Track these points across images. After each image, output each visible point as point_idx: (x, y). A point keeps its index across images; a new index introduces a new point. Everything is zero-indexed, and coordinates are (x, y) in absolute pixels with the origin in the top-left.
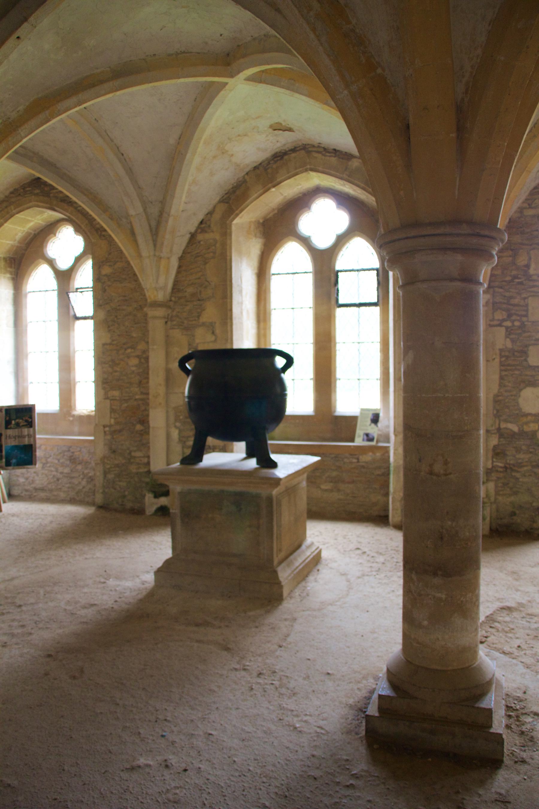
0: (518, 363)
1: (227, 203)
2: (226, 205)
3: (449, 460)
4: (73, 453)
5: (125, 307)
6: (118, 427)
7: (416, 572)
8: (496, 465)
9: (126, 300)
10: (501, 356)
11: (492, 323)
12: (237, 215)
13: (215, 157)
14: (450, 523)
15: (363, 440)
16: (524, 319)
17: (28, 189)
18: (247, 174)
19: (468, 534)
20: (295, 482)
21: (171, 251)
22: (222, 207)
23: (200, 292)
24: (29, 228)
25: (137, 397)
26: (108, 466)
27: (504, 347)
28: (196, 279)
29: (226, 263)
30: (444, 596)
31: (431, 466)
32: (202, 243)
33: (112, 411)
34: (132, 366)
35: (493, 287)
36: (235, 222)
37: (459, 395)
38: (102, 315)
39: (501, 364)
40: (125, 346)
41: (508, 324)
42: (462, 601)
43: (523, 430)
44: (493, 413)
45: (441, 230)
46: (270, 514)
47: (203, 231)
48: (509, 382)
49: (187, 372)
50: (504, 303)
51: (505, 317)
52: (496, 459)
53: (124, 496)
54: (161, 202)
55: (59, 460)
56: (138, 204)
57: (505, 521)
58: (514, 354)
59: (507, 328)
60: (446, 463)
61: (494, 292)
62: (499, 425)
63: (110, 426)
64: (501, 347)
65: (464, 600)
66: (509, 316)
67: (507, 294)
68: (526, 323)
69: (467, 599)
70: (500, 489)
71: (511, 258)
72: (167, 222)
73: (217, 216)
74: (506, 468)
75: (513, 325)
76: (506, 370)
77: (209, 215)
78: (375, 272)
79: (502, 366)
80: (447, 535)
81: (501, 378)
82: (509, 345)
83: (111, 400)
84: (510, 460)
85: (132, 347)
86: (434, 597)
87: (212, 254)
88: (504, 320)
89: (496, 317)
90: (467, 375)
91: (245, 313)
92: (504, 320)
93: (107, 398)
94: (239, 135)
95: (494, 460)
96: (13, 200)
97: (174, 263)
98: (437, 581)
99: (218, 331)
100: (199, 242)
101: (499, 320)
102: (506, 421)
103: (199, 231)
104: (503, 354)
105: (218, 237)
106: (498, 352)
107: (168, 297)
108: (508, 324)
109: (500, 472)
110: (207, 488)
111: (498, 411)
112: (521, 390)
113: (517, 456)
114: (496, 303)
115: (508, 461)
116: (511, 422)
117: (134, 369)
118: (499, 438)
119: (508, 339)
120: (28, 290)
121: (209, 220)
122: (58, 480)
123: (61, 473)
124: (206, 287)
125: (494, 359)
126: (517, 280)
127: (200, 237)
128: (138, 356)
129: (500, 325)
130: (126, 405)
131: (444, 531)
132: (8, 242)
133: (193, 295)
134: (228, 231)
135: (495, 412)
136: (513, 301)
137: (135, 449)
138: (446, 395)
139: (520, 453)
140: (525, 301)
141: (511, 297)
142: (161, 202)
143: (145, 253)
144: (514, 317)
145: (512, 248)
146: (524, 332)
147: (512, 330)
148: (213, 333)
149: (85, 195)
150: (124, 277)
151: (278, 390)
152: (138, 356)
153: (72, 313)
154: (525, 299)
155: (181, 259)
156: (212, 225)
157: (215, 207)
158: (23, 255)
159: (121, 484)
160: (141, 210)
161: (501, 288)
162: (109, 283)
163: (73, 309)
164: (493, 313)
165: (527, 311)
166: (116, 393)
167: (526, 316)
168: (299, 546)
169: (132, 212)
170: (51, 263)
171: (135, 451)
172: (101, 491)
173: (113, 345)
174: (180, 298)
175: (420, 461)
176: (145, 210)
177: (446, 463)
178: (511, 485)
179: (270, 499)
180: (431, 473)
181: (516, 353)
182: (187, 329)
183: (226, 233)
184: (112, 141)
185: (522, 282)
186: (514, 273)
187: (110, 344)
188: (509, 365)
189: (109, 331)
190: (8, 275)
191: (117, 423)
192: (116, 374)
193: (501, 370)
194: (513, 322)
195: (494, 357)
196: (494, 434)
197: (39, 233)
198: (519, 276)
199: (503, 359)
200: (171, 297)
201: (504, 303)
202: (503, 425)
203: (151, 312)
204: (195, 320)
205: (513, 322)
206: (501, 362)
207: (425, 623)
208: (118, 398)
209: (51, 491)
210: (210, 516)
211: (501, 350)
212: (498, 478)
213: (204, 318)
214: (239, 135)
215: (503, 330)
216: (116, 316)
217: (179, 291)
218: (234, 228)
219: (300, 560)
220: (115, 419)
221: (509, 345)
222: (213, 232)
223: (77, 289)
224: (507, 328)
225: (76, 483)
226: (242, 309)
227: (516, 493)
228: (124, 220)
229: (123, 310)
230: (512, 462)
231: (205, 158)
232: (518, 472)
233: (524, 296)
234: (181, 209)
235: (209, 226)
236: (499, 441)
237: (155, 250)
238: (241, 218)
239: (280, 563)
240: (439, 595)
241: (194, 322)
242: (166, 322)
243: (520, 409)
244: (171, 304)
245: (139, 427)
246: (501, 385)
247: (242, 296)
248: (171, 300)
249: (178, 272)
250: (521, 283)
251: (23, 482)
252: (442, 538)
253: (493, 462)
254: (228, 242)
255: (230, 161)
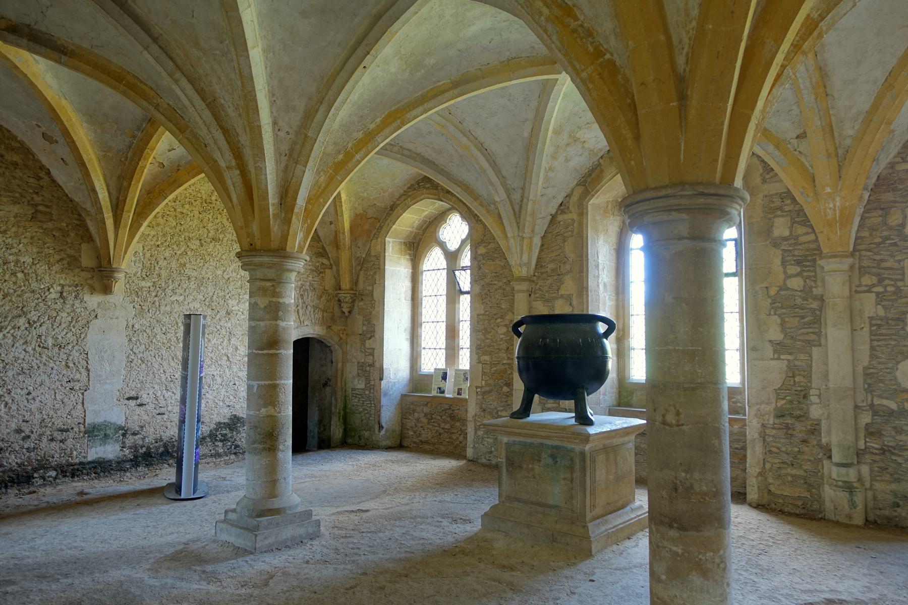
0: (894, 332)
1: (583, 185)
2: (583, 188)
3: (681, 411)
4: (453, 411)
5: (496, 282)
6: (488, 389)
7: (655, 522)
8: (870, 446)
9: (498, 276)
10: (871, 325)
11: (858, 289)
12: (593, 196)
13: (568, 145)
14: (683, 474)
15: (437, 393)
16: (900, 284)
17: (421, 184)
18: (602, 157)
19: (705, 488)
20: (616, 441)
21: (533, 231)
22: (580, 190)
23: (560, 267)
24: (425, 217)
25: (504, 362)
26: (478, 424)
27: (875, 315)
28: (556, 256)
29: (583, 240)
30: (680, 551)
31: (664, 416)
32: (561, 223)
33: (484, 373)
34: (501, 334)
35: (859, 251)
36: (590, 202)
37: (690, 348)
38: (477, 289)
39: (872, 333)
40: (495, 317)
41: (880, 289)
42: (700, 559)
43: (904, 408)
44: (864, 387)
45: (663, 193)
46: (583, 469)
47: (563, 212)
48: (883, 353)
49: (519, 334)
50: (874, 267)
51: (875, 282)
52: (870, 439)
53: (491, 452)
54: (522, 188)
55: (441, 417)
56: (502, 191)
57: (887, 513)
58: (888, 323)
59: (878, 294)
60: (678, 414)
61: (860, 256)
62: (872, 401)
63: (481, 387)
64: (871, 315)
65: (703, 558)
66: (880, 281)
67: (878, 257)
68: (902, 288)
69: (707, 558)
70: (877, 474)
71: (881, 219)
72: (527, 205)
73: (575, 198)
74: (882, 449)
75: (886, 291)
76: (878, 340)
77: (568, 198)
78: (734, 242)
79: (873, 335)
80: (681, 487)
81: (872, 348)
82: (881, 312)
83: (483, 364)
84: (889, 442)
85: (502, 317)
86: (671, 550)
87: (570, 233)
88: (874, 286)
89: (864, 283)
90: (699, 328)
91: (601, 287)
92: (874, 286)
93: (480, 362)
94: (588, 123)
95: (867, 440)
96: (410, 194)
97: (537, 241)
98: (673, 533)
99: (574, 302)
100: (559, 222)
101: (867, 286)
102: (880, 397)
103: (559, 212)
104: (874, 322)
105: (575, 217)
106: (867, 321)
107: (532, 273)
108: (880, 289)
109: (876, 454)
110: (529, 440)
111: (869, 385)
112: (898, 363)
113: (898, 438)
114: (864, 267)
115: (886, 443)
116: (887, 398)
117: (502, 336)
118: (873, 416)
119: (879, 306)
120: (425, 268)
121: (568, 202)
122: (440, 435)
123: (443, 428)
124: (564, 263)
125: (863, 328)
126: (889, 242)
127: (560, 218)
128: (506, 326)
129: (869, 291)
130: (495, 369)
131: (678, 482)
132: (407, 229)
133: (553, 270)
134: (585, 211)
135: (866, 386)
136: (884, 265)
137: (502, 408)
138: (677, 348)
139: (901, 434)
140: (900, 264)
141: (882, 261)
142: (522, 188)
143: (510, 235)
144: (887, 282)
145: (882, 207)
146: (901, 297)
147: (884, 296)
148: (571, 304)
149: (459, 186)
150: (496, 255)
151: (600, 353)
152: (506, 326)
153: (457, 288)
154: (899, 261)
155: (543, 238)
156: (570, 207)
157: (573, 190)
158: (420, 239)
159: (488, 440)
160: (505, 196)
161: (870, 250)
162: (484, 262)
163: (459, 284)
164: (860, 279)
165: (903, 274)
166: (487, 358)
167: (903, 280)
168: (623, 507)
169: (497, 199)
170: (442, 245)
171: (501, 411)
172: (472, 446)
173: (486, 315)
174: (542, 273)
175: (655, 411)
176: (509, 196)
177: (678, 414)
178: (891, 470)
179: (583, 454)
180: (664, 423)
181: (890, 322)
182: (548, 301)
183: (582, 212)
184: (476, 139)
185: (896, 242)
186: (885, 233)
187: (483, 315)
188: (881, 335)
189: (483, 303)
190: (408, 257)
191: (487, 385)
192: (488, 341)
193: (871, 340)
194: (885, 287)
195: (863, 326)
196: (866, 411)
197: (433, 221)
198: (892, 237)
199: (874, 328)
200: (534, 272)
201: (874, 267)
202: (877, 401)
203: (518, 287)
204: (555, 293)
205: (885, 287)
206: (871, 331)
207: (664, 577)
208: (488, 363)
209: (434, 444)
210: (530, 466)
211: (871, 318)
212: (874, 461)
213: (562, 292)
214: (588, 123)
215: (873, 296)
216: (489, 291)
217: (542, 266)
218: (590, 208)
219: (620, 521)
220: (486, 381)
221: (881, 312)
222: (571, 213)
223: (463, 267)
224: (878, 294)
225: (455, 438)
226: (598, 282)
227: (898, 480)
228: (492, 206)
229: (495, 284)
230: (890, 444)
231: (558, 146)
232: (899, 456)
233: (897, 258)
234: (539, 194)
235: (568, 208)
236: (873, 419)
237: (519, 231)
238: (597, 198)
239: (595, 519)
240: (674, 549)
241: (554, 295)
242: (530, 295)
243: (899, 385)
244: (535, 278)
245: (505, 389)
246: (872, 357)
247: (598, 270)
248: (534, 276)
249: (541, 250)
250: (895, 244)
251: (412, 435)
252: (676, 489)
253: (866, 442)
254: (585, 221)
255: (583, 147)
